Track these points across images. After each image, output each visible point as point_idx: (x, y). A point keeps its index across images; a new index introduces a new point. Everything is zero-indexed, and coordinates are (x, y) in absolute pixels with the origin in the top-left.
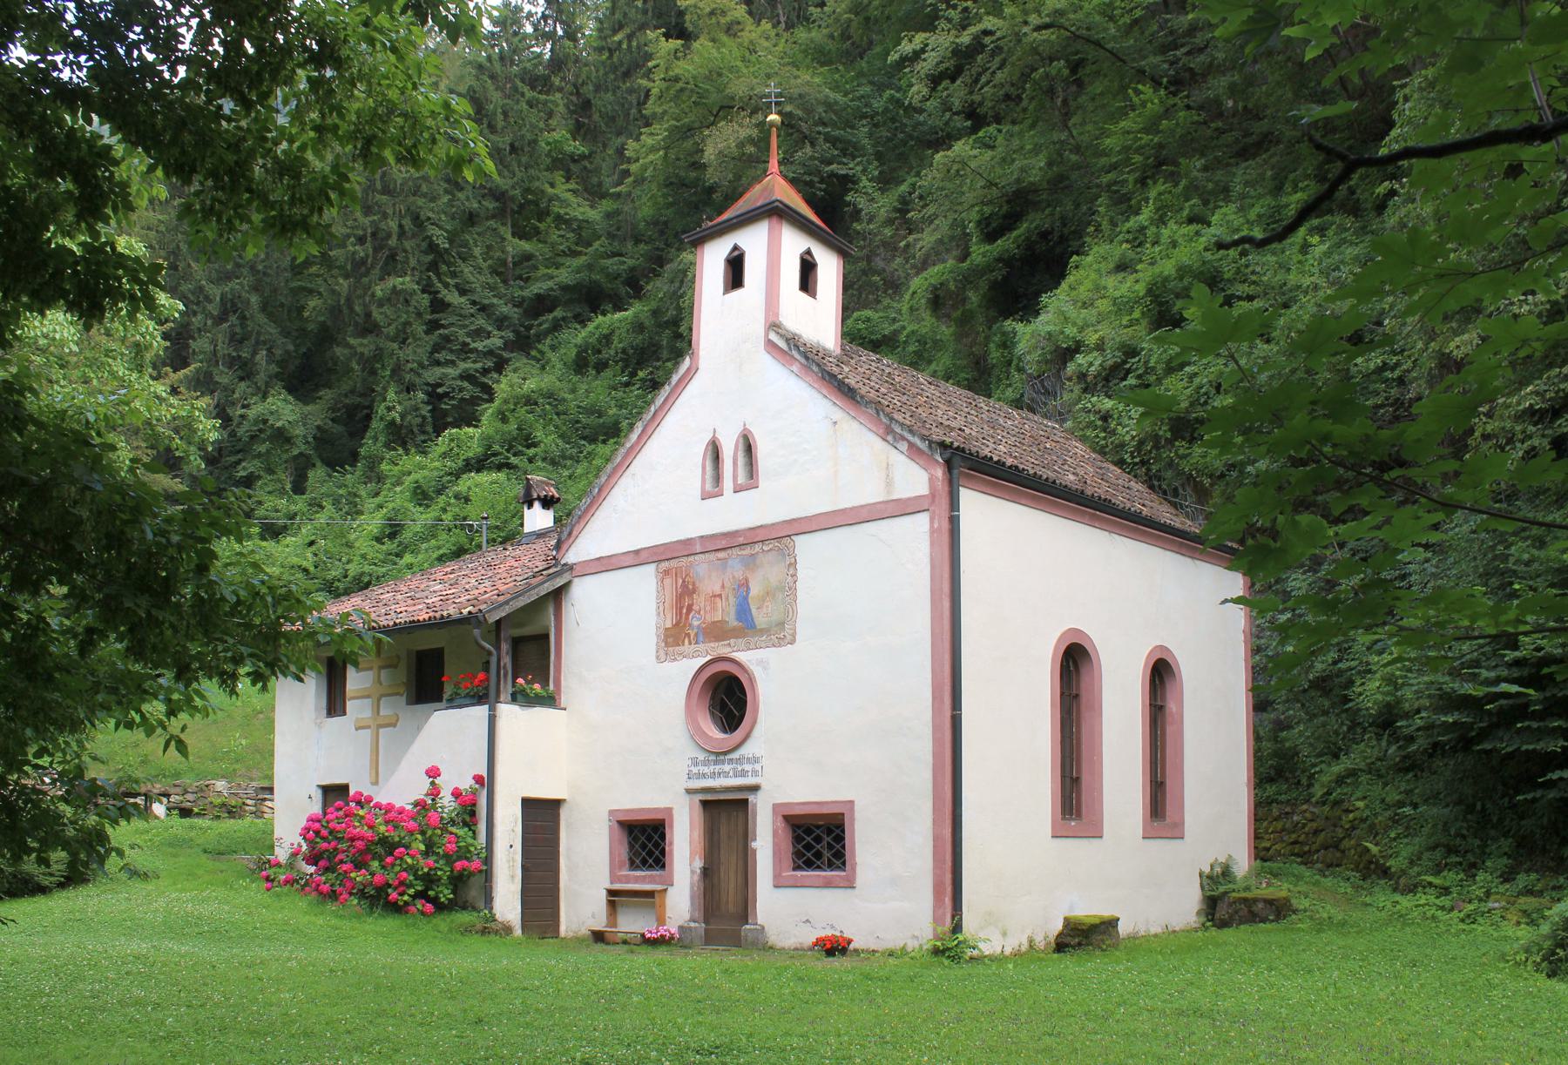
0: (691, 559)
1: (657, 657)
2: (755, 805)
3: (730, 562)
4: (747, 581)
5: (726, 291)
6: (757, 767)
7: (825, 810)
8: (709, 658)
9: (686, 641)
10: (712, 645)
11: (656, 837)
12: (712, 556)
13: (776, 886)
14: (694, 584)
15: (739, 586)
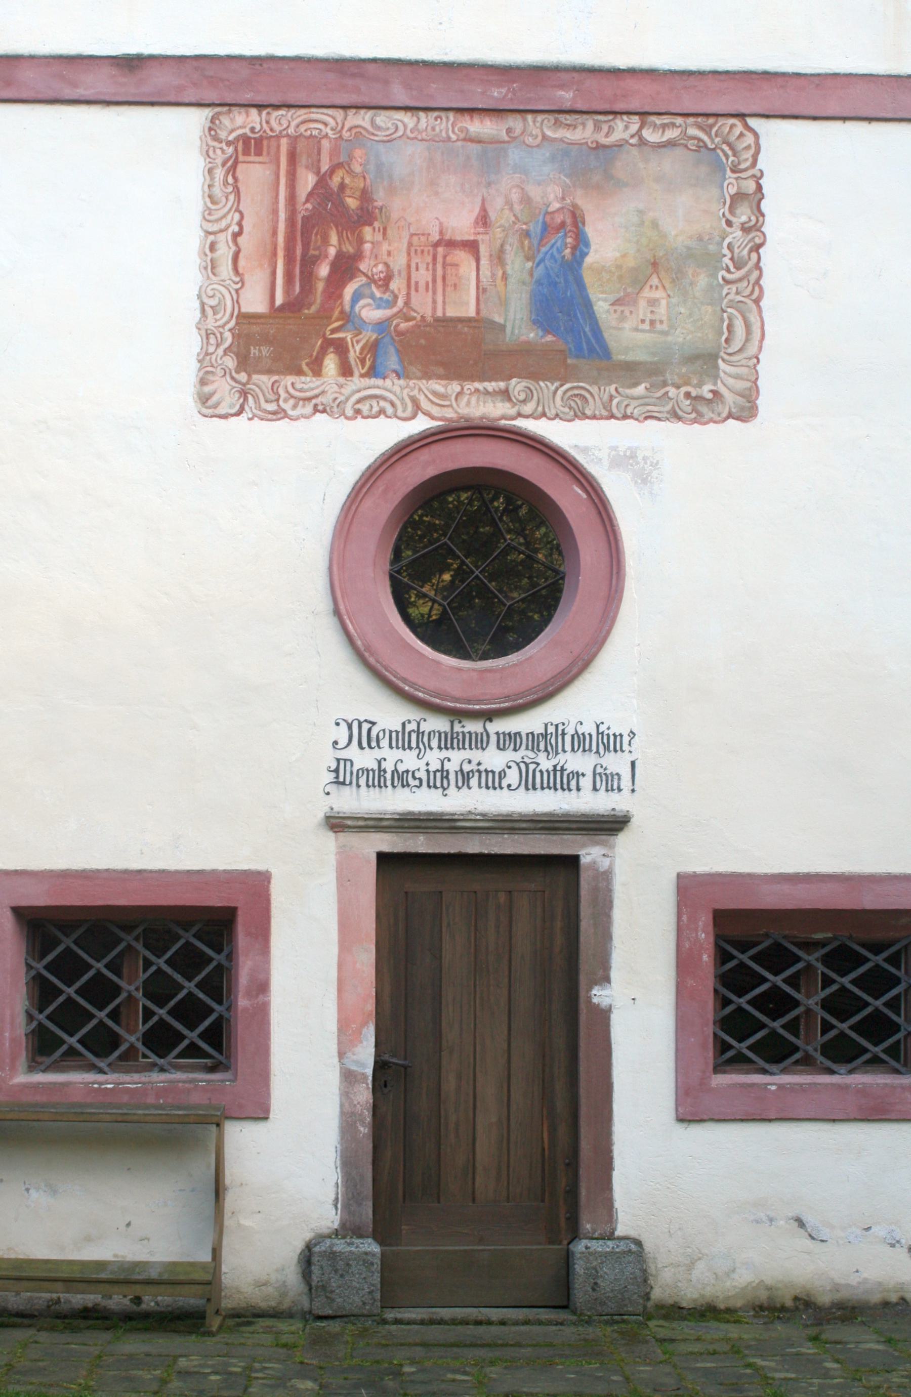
0: (363, 119)
1: (204, 399)
2: (607, 876)
3: (514, 155)
4: (577, 219)
5: (18, 911)
6: (616, 763)
7: (869, 901)
8: (420, 425)
9: (331, 364)
10: (437, 386)
11: (192, 1036)
12: (445, 125)
13: (681, 1120)
14: (365, 196)
15: (547, 229)
